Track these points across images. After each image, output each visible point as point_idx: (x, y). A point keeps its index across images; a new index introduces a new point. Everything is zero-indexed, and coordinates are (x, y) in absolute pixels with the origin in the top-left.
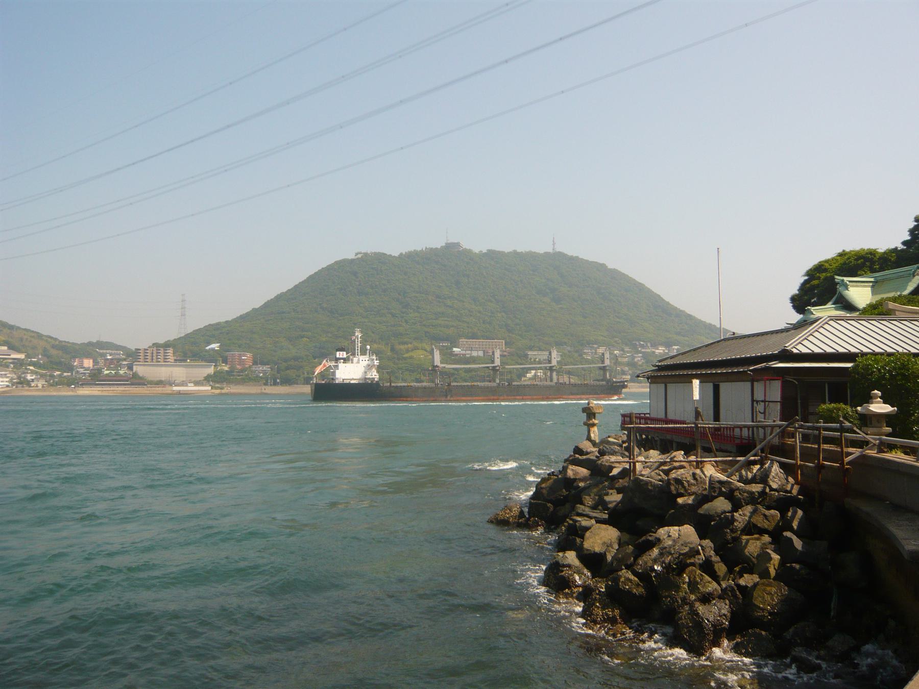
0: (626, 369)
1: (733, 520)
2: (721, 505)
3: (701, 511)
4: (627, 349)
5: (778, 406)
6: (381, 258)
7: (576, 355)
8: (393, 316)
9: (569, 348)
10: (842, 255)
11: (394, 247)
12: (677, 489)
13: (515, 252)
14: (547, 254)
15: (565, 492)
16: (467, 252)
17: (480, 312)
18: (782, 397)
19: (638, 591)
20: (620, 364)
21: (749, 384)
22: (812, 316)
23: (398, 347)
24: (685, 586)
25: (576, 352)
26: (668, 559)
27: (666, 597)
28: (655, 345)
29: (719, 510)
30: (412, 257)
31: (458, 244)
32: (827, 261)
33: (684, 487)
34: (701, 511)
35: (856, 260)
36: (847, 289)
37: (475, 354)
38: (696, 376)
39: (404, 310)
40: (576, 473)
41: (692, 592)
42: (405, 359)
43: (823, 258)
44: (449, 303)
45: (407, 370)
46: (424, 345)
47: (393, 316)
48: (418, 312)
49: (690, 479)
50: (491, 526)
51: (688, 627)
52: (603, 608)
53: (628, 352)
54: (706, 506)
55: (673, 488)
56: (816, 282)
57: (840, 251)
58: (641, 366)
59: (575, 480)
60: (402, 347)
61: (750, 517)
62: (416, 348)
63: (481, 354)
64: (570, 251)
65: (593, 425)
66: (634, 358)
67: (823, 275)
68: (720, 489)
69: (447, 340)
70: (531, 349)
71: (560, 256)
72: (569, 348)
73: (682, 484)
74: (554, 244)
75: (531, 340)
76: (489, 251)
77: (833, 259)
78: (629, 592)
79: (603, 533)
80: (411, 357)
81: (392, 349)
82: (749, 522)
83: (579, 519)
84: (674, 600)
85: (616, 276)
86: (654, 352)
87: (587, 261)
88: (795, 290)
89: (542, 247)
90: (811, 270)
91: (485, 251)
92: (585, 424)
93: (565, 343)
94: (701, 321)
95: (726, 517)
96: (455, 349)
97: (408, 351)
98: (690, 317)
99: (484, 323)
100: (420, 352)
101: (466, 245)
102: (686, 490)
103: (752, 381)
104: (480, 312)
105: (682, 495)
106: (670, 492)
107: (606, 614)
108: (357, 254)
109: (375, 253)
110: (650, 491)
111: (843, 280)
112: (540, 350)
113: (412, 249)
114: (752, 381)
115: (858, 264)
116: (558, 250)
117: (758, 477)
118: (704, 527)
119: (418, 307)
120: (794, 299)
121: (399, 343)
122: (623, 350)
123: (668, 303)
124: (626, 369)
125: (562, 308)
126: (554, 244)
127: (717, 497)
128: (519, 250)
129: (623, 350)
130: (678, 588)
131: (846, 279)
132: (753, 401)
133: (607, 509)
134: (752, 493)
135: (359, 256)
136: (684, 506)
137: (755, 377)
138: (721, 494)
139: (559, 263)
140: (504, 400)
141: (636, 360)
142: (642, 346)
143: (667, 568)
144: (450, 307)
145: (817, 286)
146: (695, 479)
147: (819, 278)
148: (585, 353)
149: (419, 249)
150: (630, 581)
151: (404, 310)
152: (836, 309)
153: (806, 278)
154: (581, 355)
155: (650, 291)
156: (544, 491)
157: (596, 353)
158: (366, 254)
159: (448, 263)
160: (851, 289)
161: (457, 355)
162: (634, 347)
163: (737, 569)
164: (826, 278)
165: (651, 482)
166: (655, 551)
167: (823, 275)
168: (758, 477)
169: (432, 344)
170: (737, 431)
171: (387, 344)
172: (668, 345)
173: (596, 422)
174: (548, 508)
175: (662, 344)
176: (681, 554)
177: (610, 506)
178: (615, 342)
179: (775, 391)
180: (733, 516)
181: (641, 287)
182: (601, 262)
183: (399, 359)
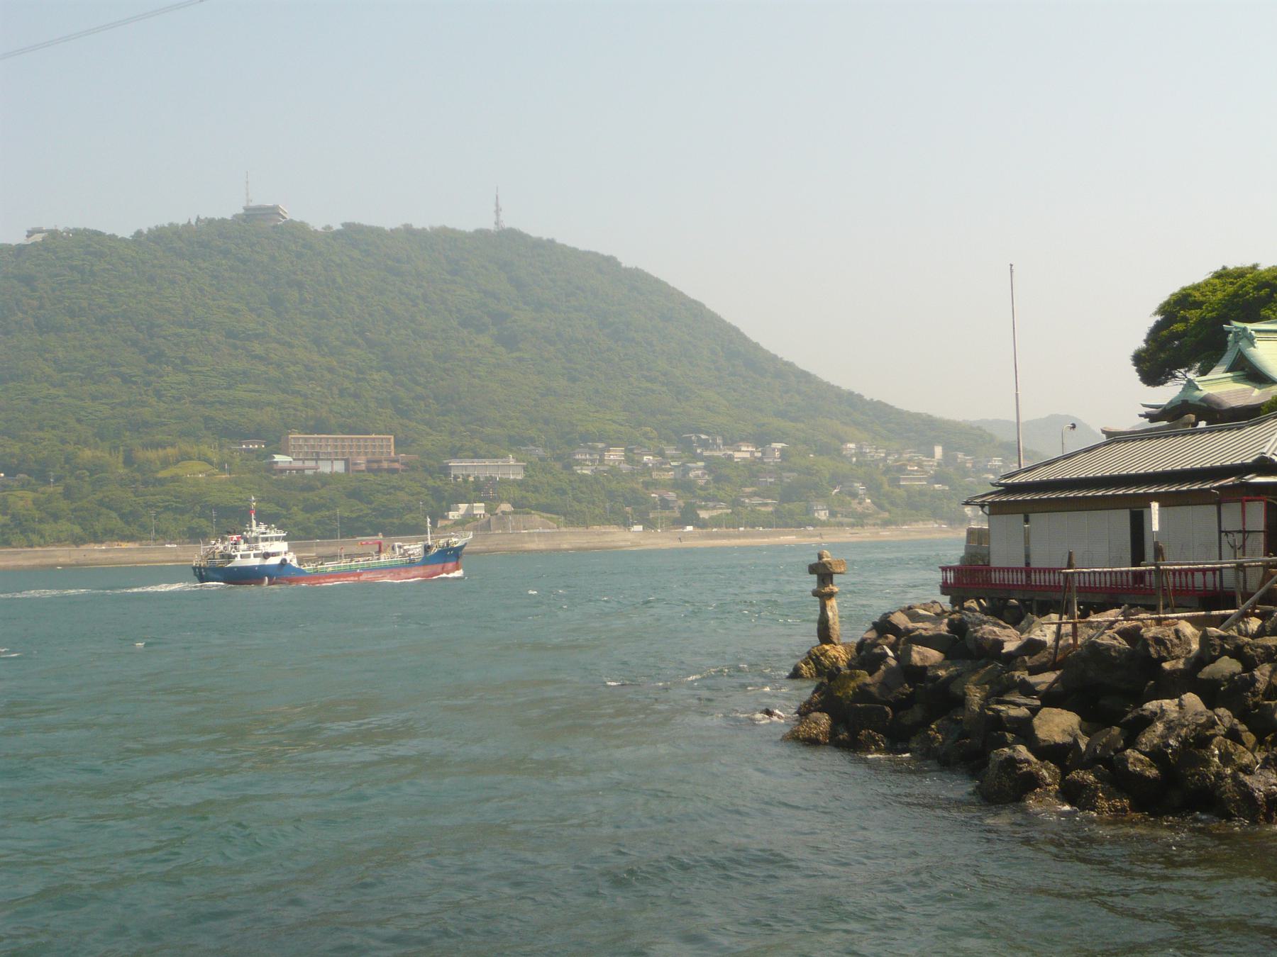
0: (671, 495)
1: (1254, 680)
2: (1227, 666)
3: (1201, 675)
4: (670, 451)
5: (1262, 537)
6: (91, 245)
7: (558, 466)
8: (126, 380)
9: (540, 451)
10: (1223, 275)
11: (123, 215)
12: (1158, 652)
13: (409, 231)
14: (481, 234)
15: (907, 689)
16: (297, 231)
17: (331, 370)
18: (1268, 526)
19: (1152, 772)
20: (655, 484)
21: (1215, 508)
22: (1197, 393)
23: (142, 455)
24: (1216, 759)
25: (558, 458)
26: (1183, 732)
27: (1193, 776)
28: (732, 442)
29: (1227, 673)
30: (167, 244)
31: (274, 211)
32: (1196, 287)
33: (1167, 648)
34: (1201, 675)
35: (1257, 289)
36: (1252, 344)
37: (325, 468)
38: (1156, 497)
39: (151, 367)
40: (924, 658)
41: (1225, 766)
42: (161, 482)
43: (1188, 282)
44: (258, 349)
45: (167, 508)
46: (204, 448)
47: (126, 380)
48: (188, 372)
49: (1172, 637)
50: (785, 750)
51: (1235, 801)
52: (1108, 799)
53: (673, 458)
54: (1207, 669)
55: (1152, 650)
56: (1179, 327)
57: (1218, 268)
58: (702, 488)
59: (924, 668)
60: (151, 454)
61: (1270, 677)
62: (186, 457)
63: (339, 467)
64: (536, 227)
65: (831, 595)
66: (686, 471)
67: (1194, 315)
68: (1222, 646)
69: (256, 435)
70: (455, 454)
71: (512, 237)
72: (540, 451)
73: (1165, 645)
74: (498, 211)
75: (452, 433)
76: (348, 226)
77: (1207, 283)
78: (1141, 776)
79: (1057, 720)
80: (175, 479)
81: (129, 461)
82: (1270, 683)
83: (1002, 708)
84: (1204, 777)
85: (640, 284)
86: (730, 458)
87: (574, 250)
88: (1138, 341)
89: (469, 216)
90: (1167, 303)
91: (337, 226)
92: (815, 594)
93: (532, 441)
94: (830, 387)
95: (1245, 679)
96: (278, 458)
97: (166, 463)
98: (805, 376)
99: (342, 392)
100: (197, 466)
101: (293, 212)
102: (1169, 653)
103: (1219, 504)
104: (331, 370)
105: (1165, 660)
106: (1149, 656)
107: (1114, 806)
108: (31, 234)
109: (77, 232)
110: (1115, 658)
111: (1245, 329)
112: (477, 456)
113: (164, 221)
114: (1219, 504)
115: (1260, 297)
116: (507, 224)
117: (1268, 629)
118: (1212, 694)
119: (185, 361)
120: (1139, 359)
121: (146, 447)
122: (661, 453)
123: (756, 347)
124: (671, 495)
125: (520, 360)
126: (498, 211)
127: (1219, 657)
128: (417, 225)
129: (661, 453)
130: (1207, 763)
131: (1250, 327)
132: (1220, 532)
133: (1036, 693)
134: (1267, 648)
135: (38, 238)
136: (1173, 672)
137: (1220, 499)
138: (1224, 652)
139: (507, 252)
140: (84, 594)
141: (692, 475)
142: (705, 445)
143: (1184, 742)
144: (261, 358)
145: (1178, 336)
146: (1178, 637)
147: (1185, 319)
148: (579, 463)
149: (181, 220)
150: (1141, 761)
151: (151, 367)
152: (1236, 380)
153: (1159, 318)
154: (568, 467)
155: (716, 320)
156: (873, 689)
157: (601, 461)
158: (53, 234)
159: (251, 251)
160: (1258, 344)
161: (282, 471)
162: (686, 446)
163: (1269, 738)
164: (1202, 322)
165: (1114, 646)
166: (1160, 727)
167: (1194, 315)
168: (1268, 629)
169: (221, 446)
170: (1198, 576)
171: (116, 448)
172: (761, 440)
173: (836, 589)
174: (887, 713)
175: (745, 440)
176: (1198, 725)
177: (1038, 688)
178: (645, 434)
179: (1257, 515)
180: (1253, 676)
181: (696, 311)
182: (606, 252)
183: (146, 483)
